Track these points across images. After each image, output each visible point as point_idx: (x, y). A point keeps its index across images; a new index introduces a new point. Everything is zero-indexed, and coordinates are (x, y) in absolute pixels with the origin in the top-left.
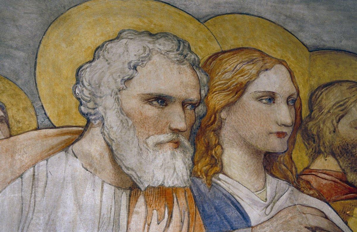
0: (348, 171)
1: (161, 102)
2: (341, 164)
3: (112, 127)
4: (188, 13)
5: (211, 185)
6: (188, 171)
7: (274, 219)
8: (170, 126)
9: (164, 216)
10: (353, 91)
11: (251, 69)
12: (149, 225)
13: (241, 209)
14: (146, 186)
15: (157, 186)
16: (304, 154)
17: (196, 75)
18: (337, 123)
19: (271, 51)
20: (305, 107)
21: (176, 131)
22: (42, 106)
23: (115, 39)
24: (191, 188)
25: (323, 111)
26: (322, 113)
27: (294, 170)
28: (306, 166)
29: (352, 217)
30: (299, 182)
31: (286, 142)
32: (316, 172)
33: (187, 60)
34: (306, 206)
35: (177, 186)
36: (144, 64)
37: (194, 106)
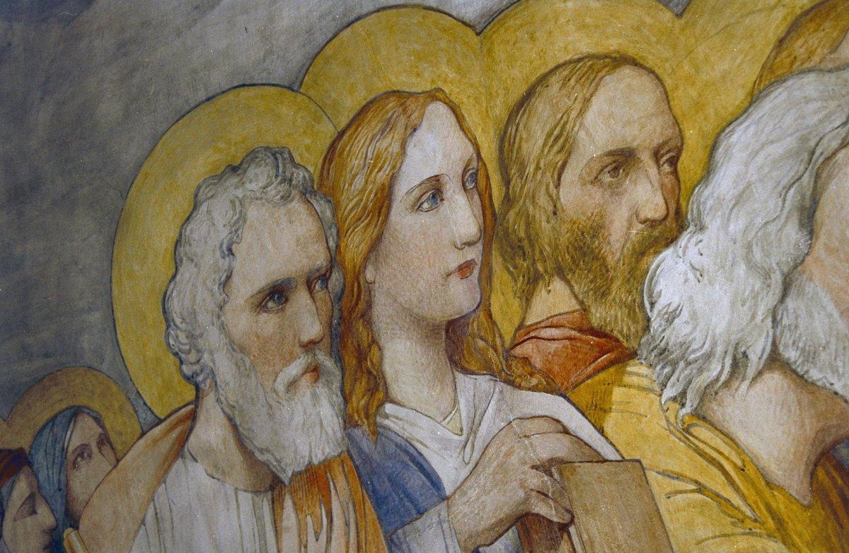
0: (589, 302)
1: (278, 298)
2: (576, 288)
3: (227, 384)
4: (274, 85)
5: (377, 432)
6: (340, 418)
7: (480, 468)
8: (299, 340)
9: (322, 522)
10: (573, 88)
11: (390, 145)
12: (306, 547)
13: (426, 466)
14: (290, 474)
15: (303, 469)
16: (511, 296)
17: (314, 212)
18: (556, 188)
19: (414, 80)
20: (495, 179)
21: (310, 346)
22: (138, 392)
23: (192, 213)
24: (348, 451)
25: (527, 172)
26: (527, 177)
27: (498, 341)
28: (517, 322)
29: (611, 412)
30: (509, 367)
31: (476, 282)
32: (537, 329)
33: (296, 187)
34: (528, 418)
35: (329, 457)
36: (240, 235)
37: (325, 278)
